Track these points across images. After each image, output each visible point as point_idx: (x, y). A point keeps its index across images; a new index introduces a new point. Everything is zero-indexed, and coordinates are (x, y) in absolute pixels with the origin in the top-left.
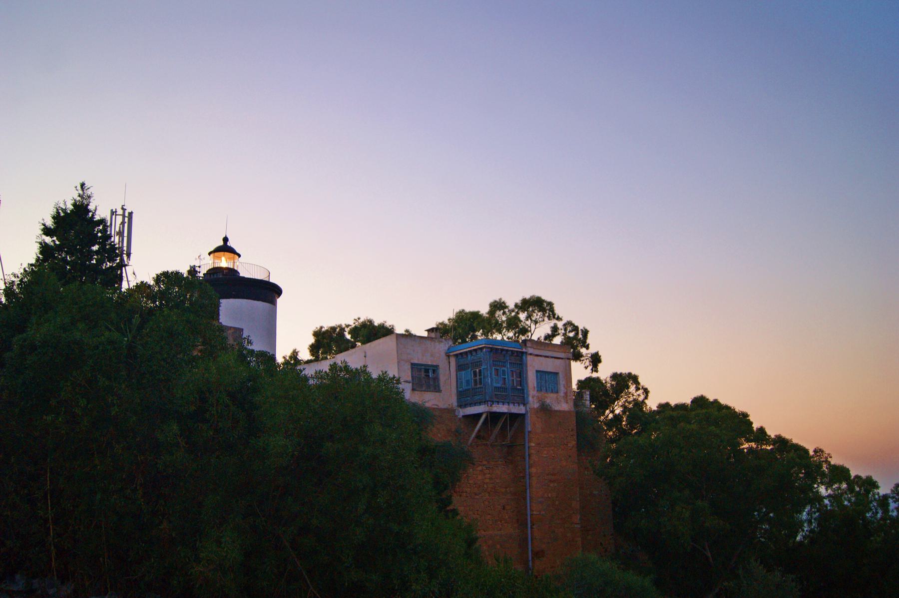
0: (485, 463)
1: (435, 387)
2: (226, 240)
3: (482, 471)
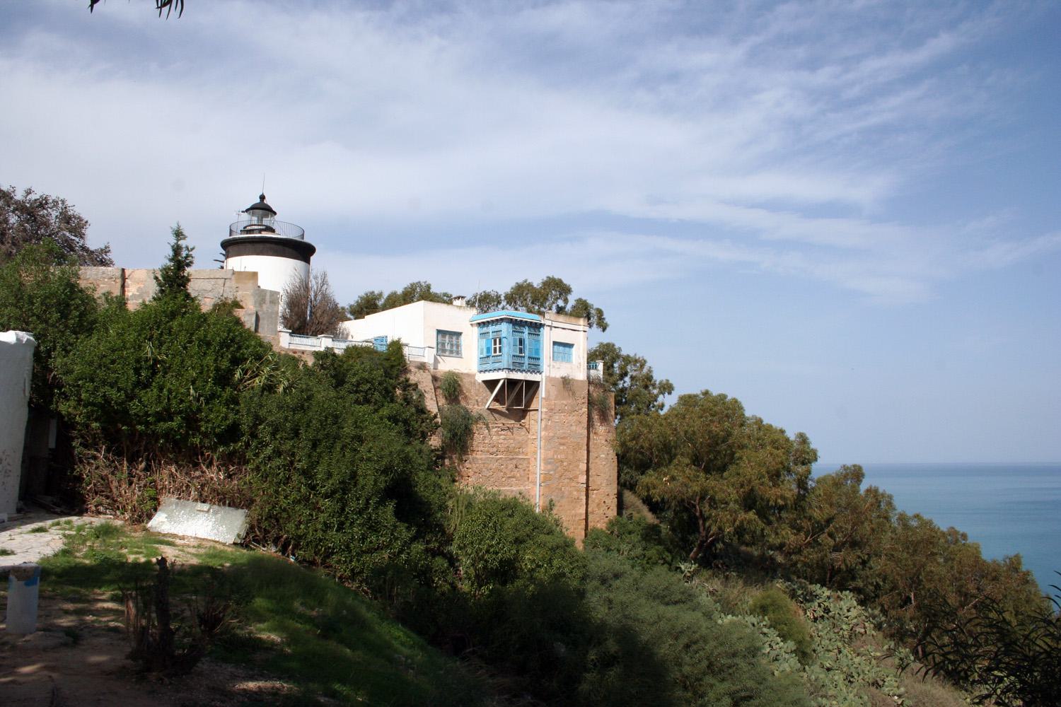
2: (262, 198)
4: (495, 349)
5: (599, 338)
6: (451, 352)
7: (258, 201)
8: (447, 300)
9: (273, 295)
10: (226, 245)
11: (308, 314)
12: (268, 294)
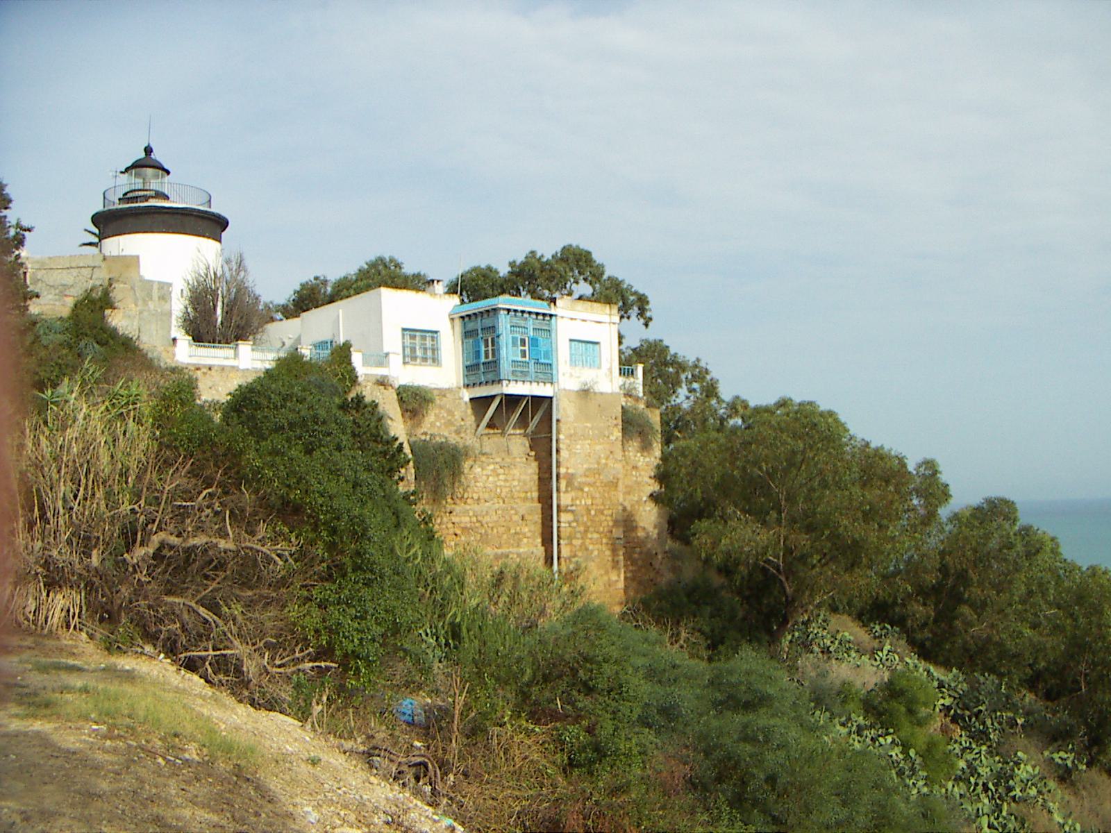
0: (498, 460)
1: (432, 357)
2: (148, 150)
3: (494, 470)
4: (486, 352)
5: (636, 333)
6: (425, 359)
7: (143, 155)
8: (419, 283)
9: (162, 288)
10: (97, 219)
11: (220, 315)
12: (156, 286)
